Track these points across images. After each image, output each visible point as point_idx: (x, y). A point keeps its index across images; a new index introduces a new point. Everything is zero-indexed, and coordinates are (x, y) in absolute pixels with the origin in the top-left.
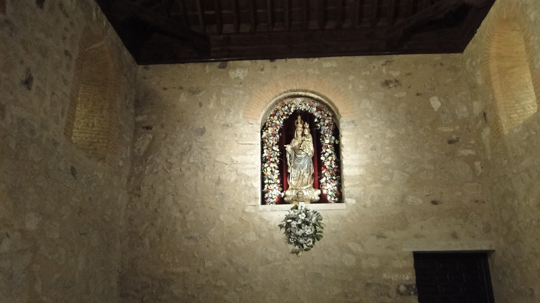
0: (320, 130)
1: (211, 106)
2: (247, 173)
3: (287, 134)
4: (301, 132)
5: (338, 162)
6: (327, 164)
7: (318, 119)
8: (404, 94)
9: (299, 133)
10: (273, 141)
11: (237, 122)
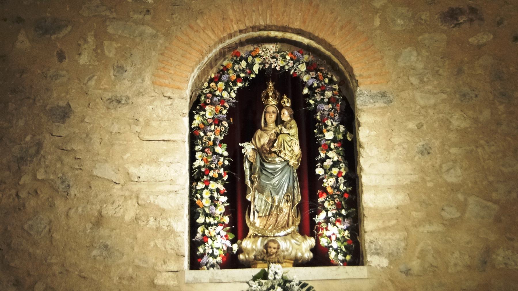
1: (84, 59)
2: (162, 201)
3: (244, 120)
5: (353, 179)
6: (329, 183)
8: (485, 38)
9: (271, 118)
10: (213, 134)
11: (139, 94)
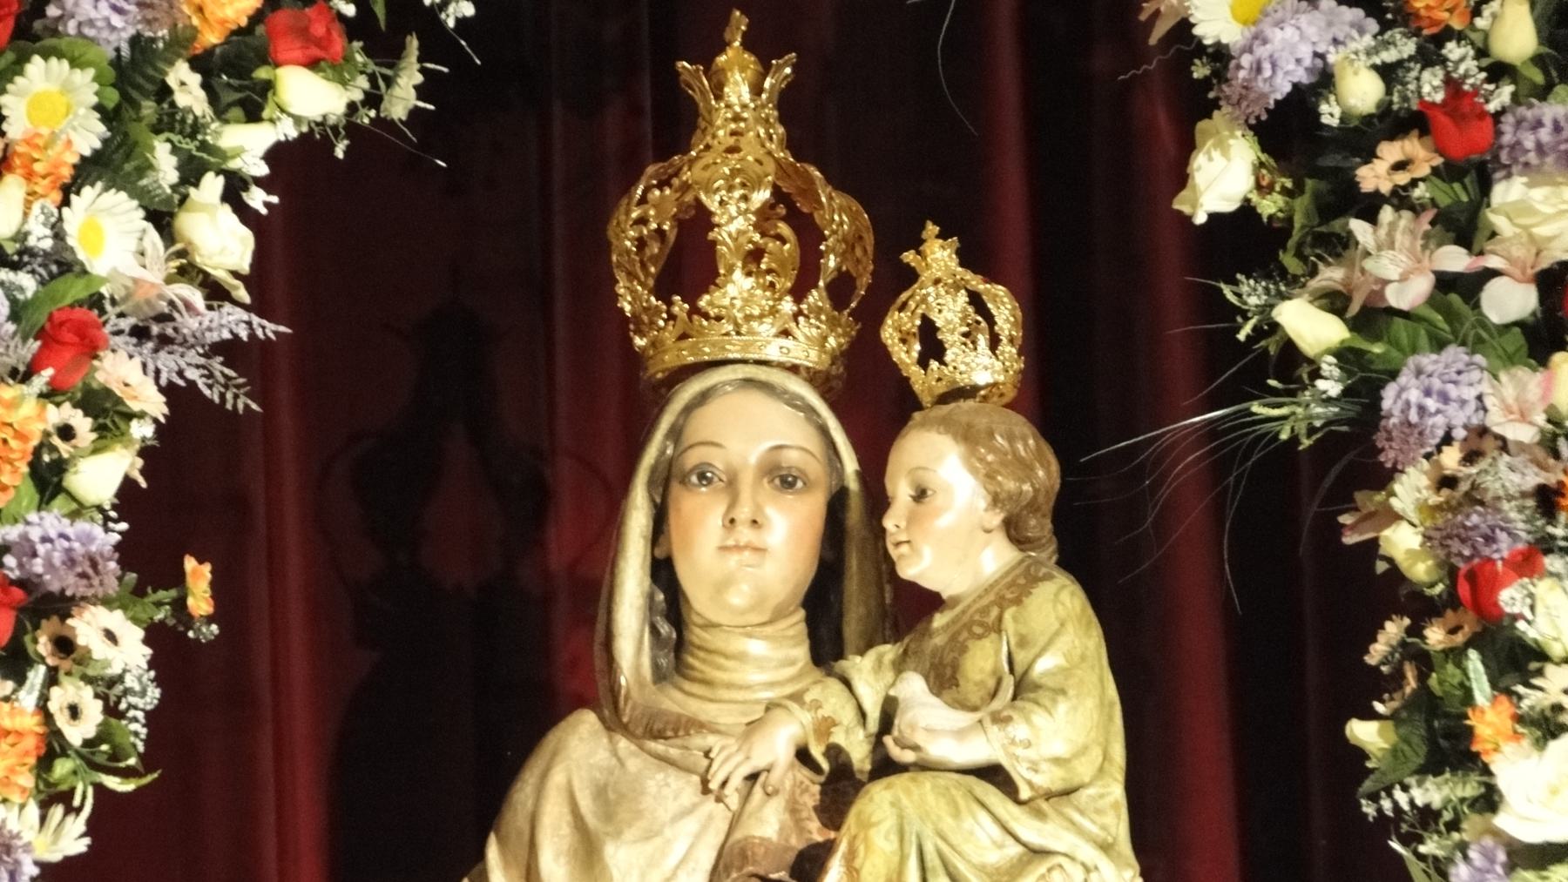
0: (1356, 455)
4: (786, 537)
7: (1291, 129)
9: (749, 557)
